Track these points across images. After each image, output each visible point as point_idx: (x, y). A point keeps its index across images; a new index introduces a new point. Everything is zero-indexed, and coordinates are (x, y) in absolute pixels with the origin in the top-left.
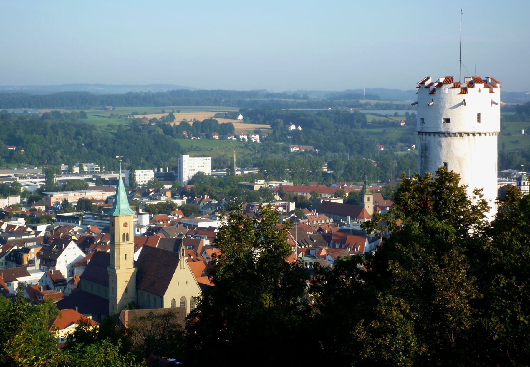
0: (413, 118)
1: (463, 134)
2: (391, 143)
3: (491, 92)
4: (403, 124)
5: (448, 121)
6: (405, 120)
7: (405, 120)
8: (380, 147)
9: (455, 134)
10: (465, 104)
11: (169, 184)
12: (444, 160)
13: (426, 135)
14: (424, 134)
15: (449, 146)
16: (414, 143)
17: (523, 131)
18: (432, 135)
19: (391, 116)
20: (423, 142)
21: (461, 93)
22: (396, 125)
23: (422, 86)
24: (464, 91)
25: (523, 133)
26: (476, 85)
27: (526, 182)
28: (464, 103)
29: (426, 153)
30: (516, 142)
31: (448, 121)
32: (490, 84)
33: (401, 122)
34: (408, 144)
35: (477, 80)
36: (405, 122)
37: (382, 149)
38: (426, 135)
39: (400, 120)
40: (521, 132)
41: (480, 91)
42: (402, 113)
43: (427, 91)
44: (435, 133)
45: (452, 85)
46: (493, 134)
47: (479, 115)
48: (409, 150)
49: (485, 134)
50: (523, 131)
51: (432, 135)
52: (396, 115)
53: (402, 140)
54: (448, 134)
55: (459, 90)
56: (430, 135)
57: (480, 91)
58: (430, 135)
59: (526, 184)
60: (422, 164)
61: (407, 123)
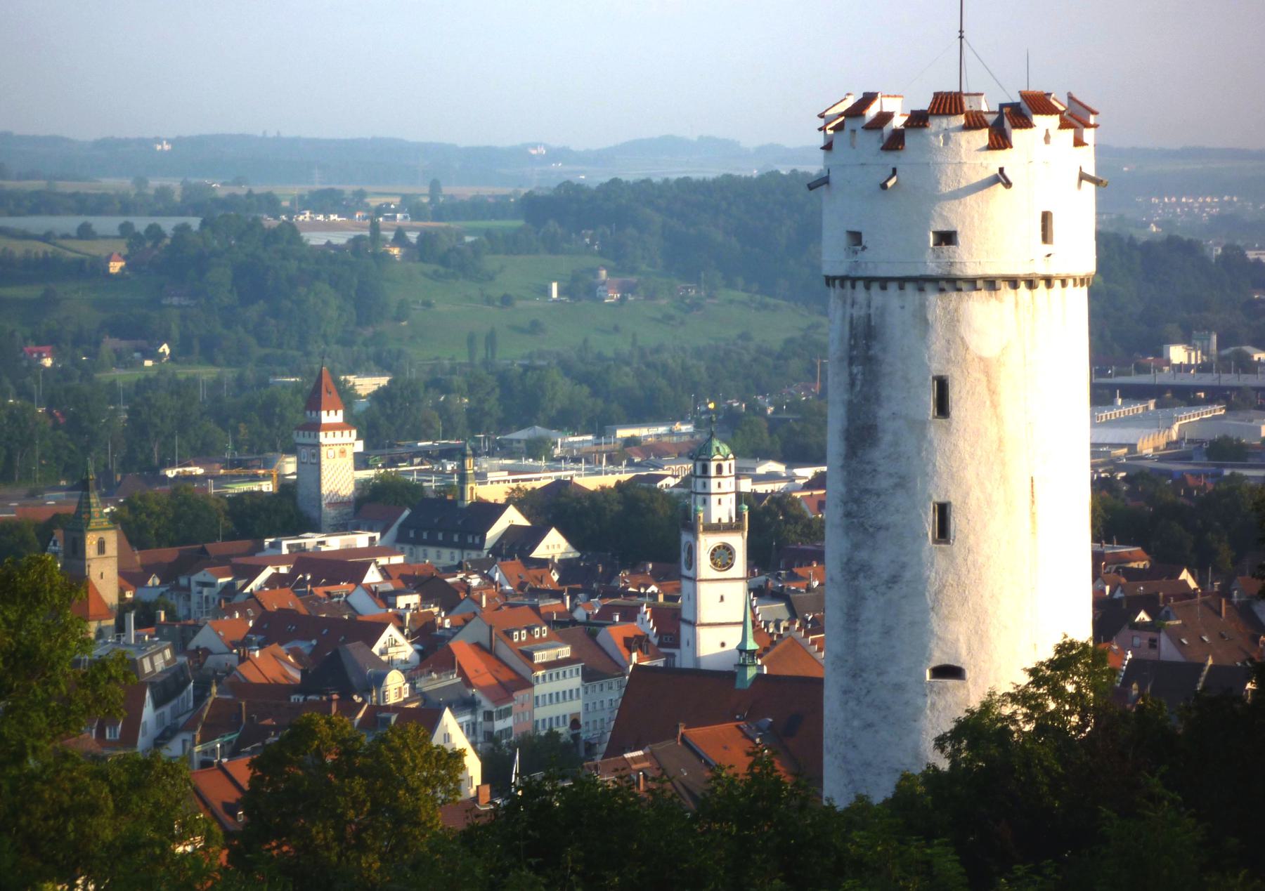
0: (155, 246)
1: (998, 282)
2: (78, 340)
3: (1079, 142)
4: (115, 267)
5: (947, 238)
6: (125, 251)
7: (125, 251)
8: (40, 357)
9: (973, 283)
10: (1008, 184)
11: (663, 425)
12: (936, 368)
13: (867, 288)
14: (860, 285)
15: (953, 322)
16: (166, 339)
17: (555, 286)
18: (893, 287)
19: (66, 237)
20: (858, 312)
21: (991, 147)
22: (92, 270)
23: (850, 124)
24: (1000, 141)
25: (555, 295)
26: (1036, 119)
27: (725, 465)
28: (1001, 178)
29: (869, 348)
30: (535, 328)
31: (947, 238)
32: (1076, 118)
33: (109, 259)
34: (142, 343)
35: (1040, 104)
36: (125, 258)
37: (48, 362)
38: (867, 288)
39: (105, 254)
40: (546, 291)
41: (1047, 138)
42: (107, 224)
43: (872, 142)
44: (902, 281)
45: (961, 120)
46: (1064, 283)
47: (1046, 217)
48: (148, 363)
49: (1064, 283)
50: (555, 286)
51: (893, 287)
52: (85, 233)
53: (117, 329)
54: (952, 283)
55: (983, 136)
56: (884, 288)
57: (1047, 138)
58: (884, 288)
59: (725, 472)
60: (852, 384)
61: (132, 264)
